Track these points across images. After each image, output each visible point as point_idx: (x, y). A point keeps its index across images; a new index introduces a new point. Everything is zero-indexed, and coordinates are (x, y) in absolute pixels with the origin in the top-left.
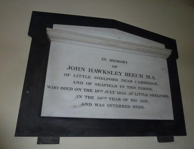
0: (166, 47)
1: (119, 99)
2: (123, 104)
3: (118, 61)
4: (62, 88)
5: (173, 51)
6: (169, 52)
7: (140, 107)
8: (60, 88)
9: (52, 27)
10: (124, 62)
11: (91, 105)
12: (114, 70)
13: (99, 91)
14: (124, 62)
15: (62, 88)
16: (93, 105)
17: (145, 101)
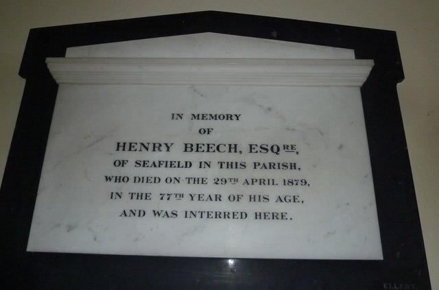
0: (358, 56)
1: (218, 198)
2: (227, 210)
3: (215, 117)
4: (137, 180)
5: (375, 62)
6: (363, 70)
7: (274, 216)
8: (132, 179)
9: (62, 54)
10: (229, 117)
11: (144, 214)
12: (205, 139)
13: (228, 181)
14: (229, 117)
15: (137, 180)
16: (149, 213)
17: (292, 201)
